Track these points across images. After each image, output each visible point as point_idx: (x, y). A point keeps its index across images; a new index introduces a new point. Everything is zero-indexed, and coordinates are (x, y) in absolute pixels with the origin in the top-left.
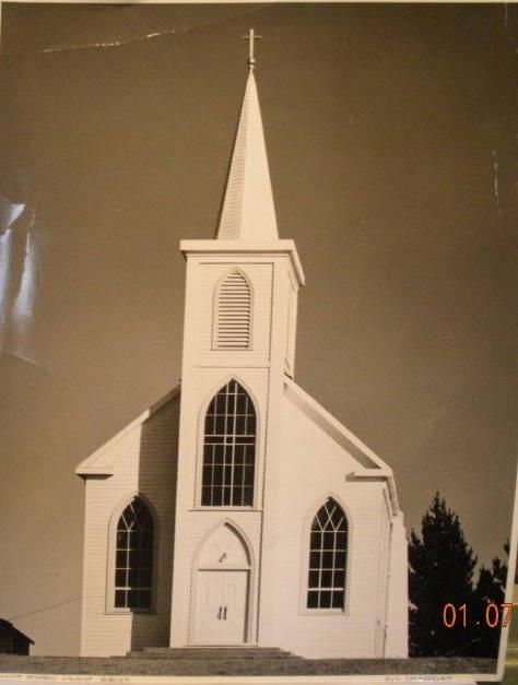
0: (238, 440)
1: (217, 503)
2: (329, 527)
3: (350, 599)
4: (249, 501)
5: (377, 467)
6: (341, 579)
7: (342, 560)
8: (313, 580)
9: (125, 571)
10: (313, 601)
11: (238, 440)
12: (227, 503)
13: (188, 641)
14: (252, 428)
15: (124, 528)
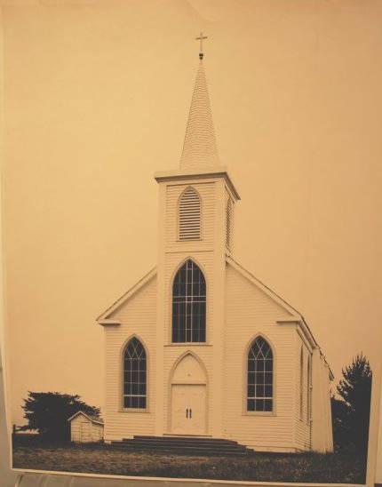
0: (184, 299)
1: (183, 341)
2: (135, 356)
3: (150, 403)
4: (203, 339)
5: (106, 318)
6: (269, 392)
7: (270, 378)
8: (250, 392)
9: (262, 386)
10: (251, 406)
11: (195, 299)
12: (189, 341)
13: (169, 427)
14: (204, 291)
15: (253, 357)
